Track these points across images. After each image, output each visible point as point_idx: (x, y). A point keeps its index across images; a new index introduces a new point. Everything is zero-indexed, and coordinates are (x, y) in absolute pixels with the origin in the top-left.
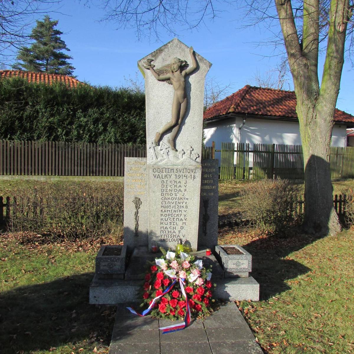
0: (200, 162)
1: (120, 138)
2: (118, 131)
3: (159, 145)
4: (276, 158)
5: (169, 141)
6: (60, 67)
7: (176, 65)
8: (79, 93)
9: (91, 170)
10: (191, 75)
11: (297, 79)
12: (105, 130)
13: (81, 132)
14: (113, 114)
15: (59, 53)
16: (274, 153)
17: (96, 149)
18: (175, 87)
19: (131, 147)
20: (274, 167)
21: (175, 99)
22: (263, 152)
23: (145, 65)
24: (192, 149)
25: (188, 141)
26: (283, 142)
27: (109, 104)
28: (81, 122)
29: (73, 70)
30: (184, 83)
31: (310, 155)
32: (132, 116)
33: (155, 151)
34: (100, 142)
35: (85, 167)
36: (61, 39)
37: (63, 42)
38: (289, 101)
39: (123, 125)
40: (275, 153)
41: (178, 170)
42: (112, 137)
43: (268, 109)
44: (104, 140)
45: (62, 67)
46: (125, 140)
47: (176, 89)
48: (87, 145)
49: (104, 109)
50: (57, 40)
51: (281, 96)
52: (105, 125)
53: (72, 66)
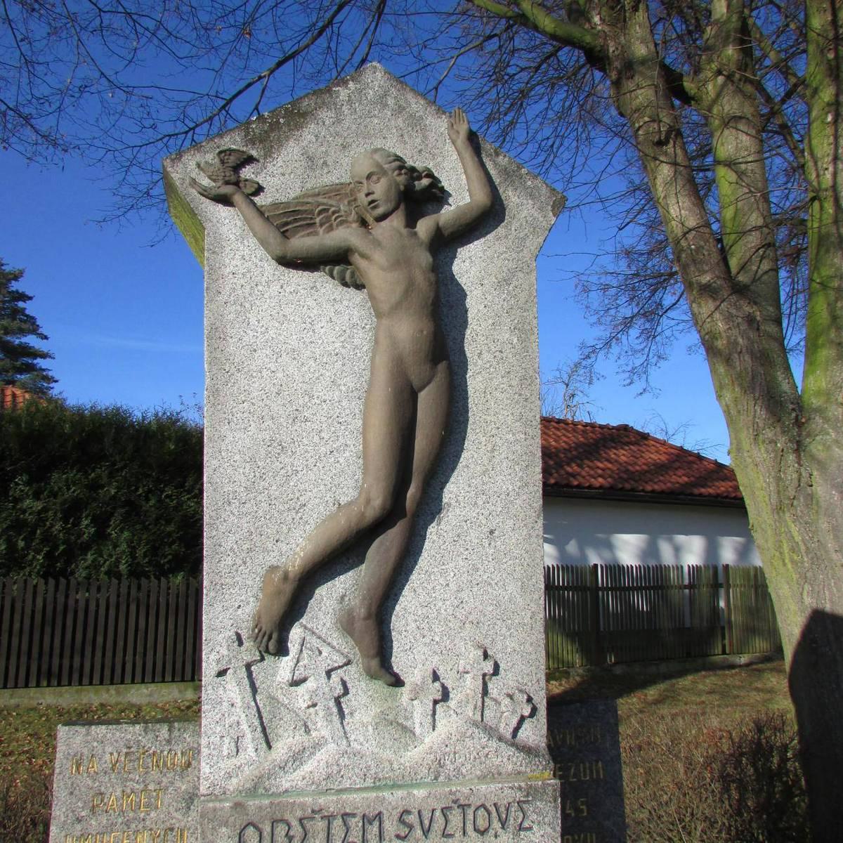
0: (543, 745)
1: (147, 560)
2: (140, 539)
3: (282, 650)
4: (604, 606)
5: (347, 625)
6: (19, 376)
7: (384, 181)
8: (23, 425)
9: (45, 667)
10: (463, 245)
11: (728, 361)
12: (101, 536)
13: (21, 544)
14: (129, 486)
15: (20, 345)
16: (598, 589)
17: (67, 596)
18: (381, 296)
19: (182, 589)
20: (602, 629)
21: (383, 362)
22: (564, 588)
23: (205, 182)
24: (488, 667)
25: (461, 614)
26: (615, 559)
27: (117, 458)
28: (24, 512)
29: (51, 385)
30: (432, 277)
31: (808, 612)
32: (189, 492)
33: (254, 690)
34: (81, 574)
35: (24, 659)
36: (27, 312)
37: (32, 320)
38: (615, 448)
39: (157, 519)
40: (600, 589)
41: (413, 819)
42: (121, 558)
43: (569, 469)
44: (95, 566)
45: (23, 377)
46: (164, 565)
47: (385, 307)
48: (35, 586)
49: (101, 472)
50: (16, 313)
51: (592, 438)
52: (101, 522)
53: (50, 374)
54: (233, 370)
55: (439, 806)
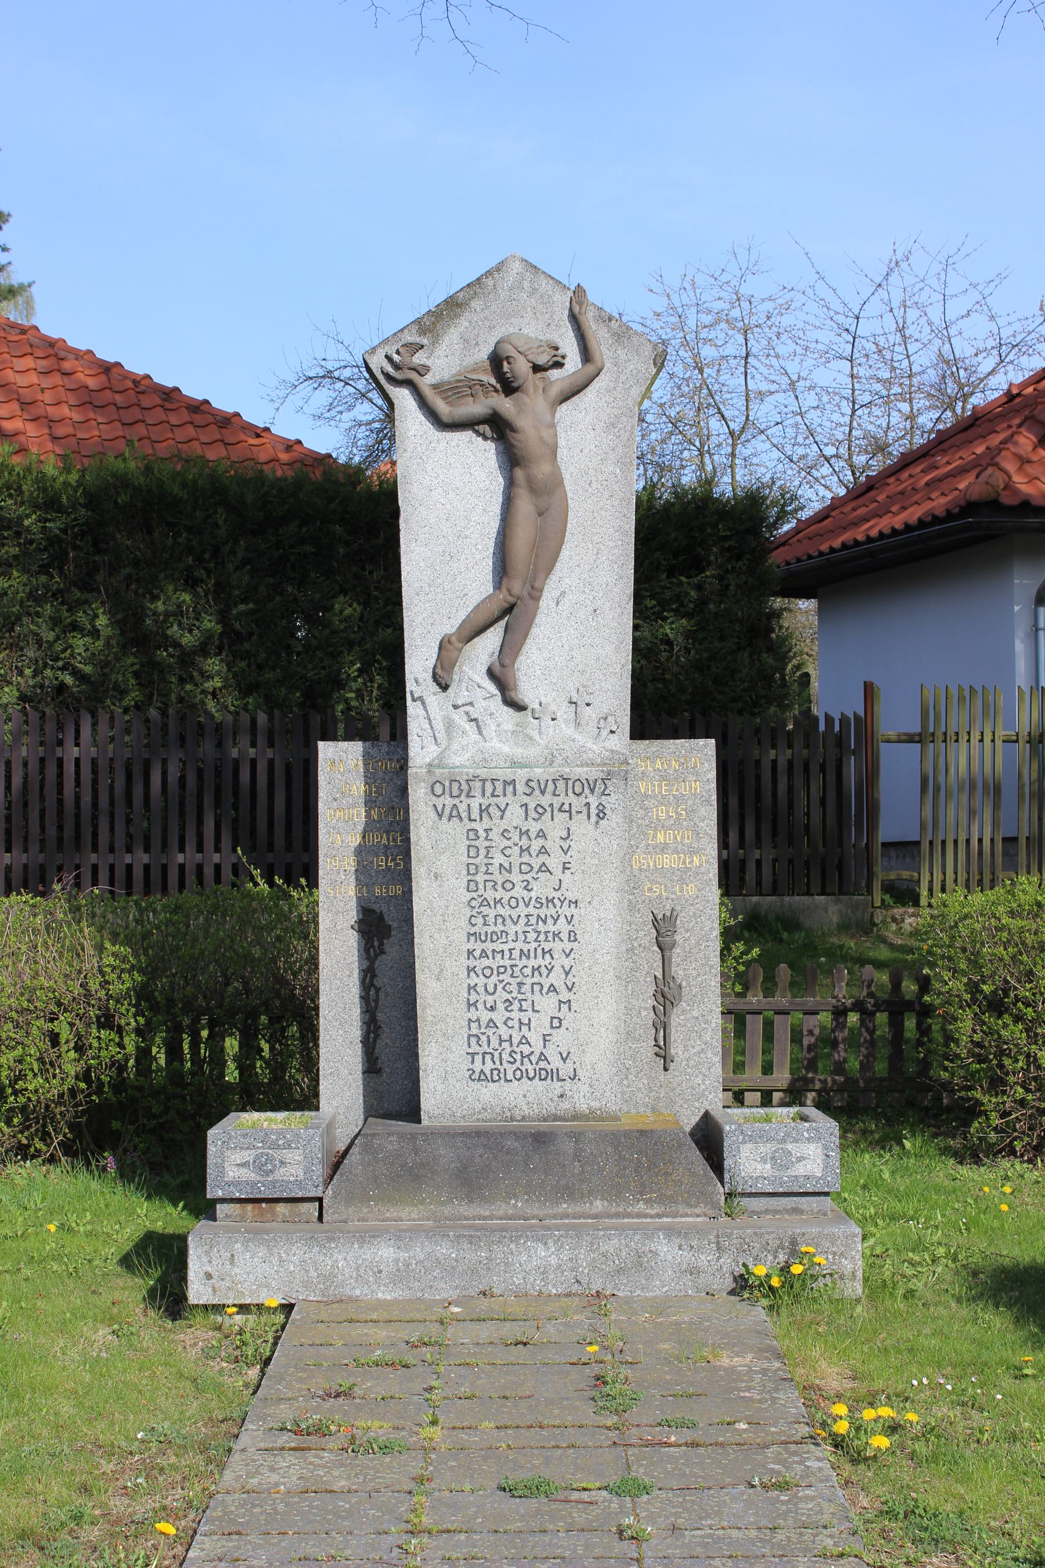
54: (417, 505)
55: (550, 778)
